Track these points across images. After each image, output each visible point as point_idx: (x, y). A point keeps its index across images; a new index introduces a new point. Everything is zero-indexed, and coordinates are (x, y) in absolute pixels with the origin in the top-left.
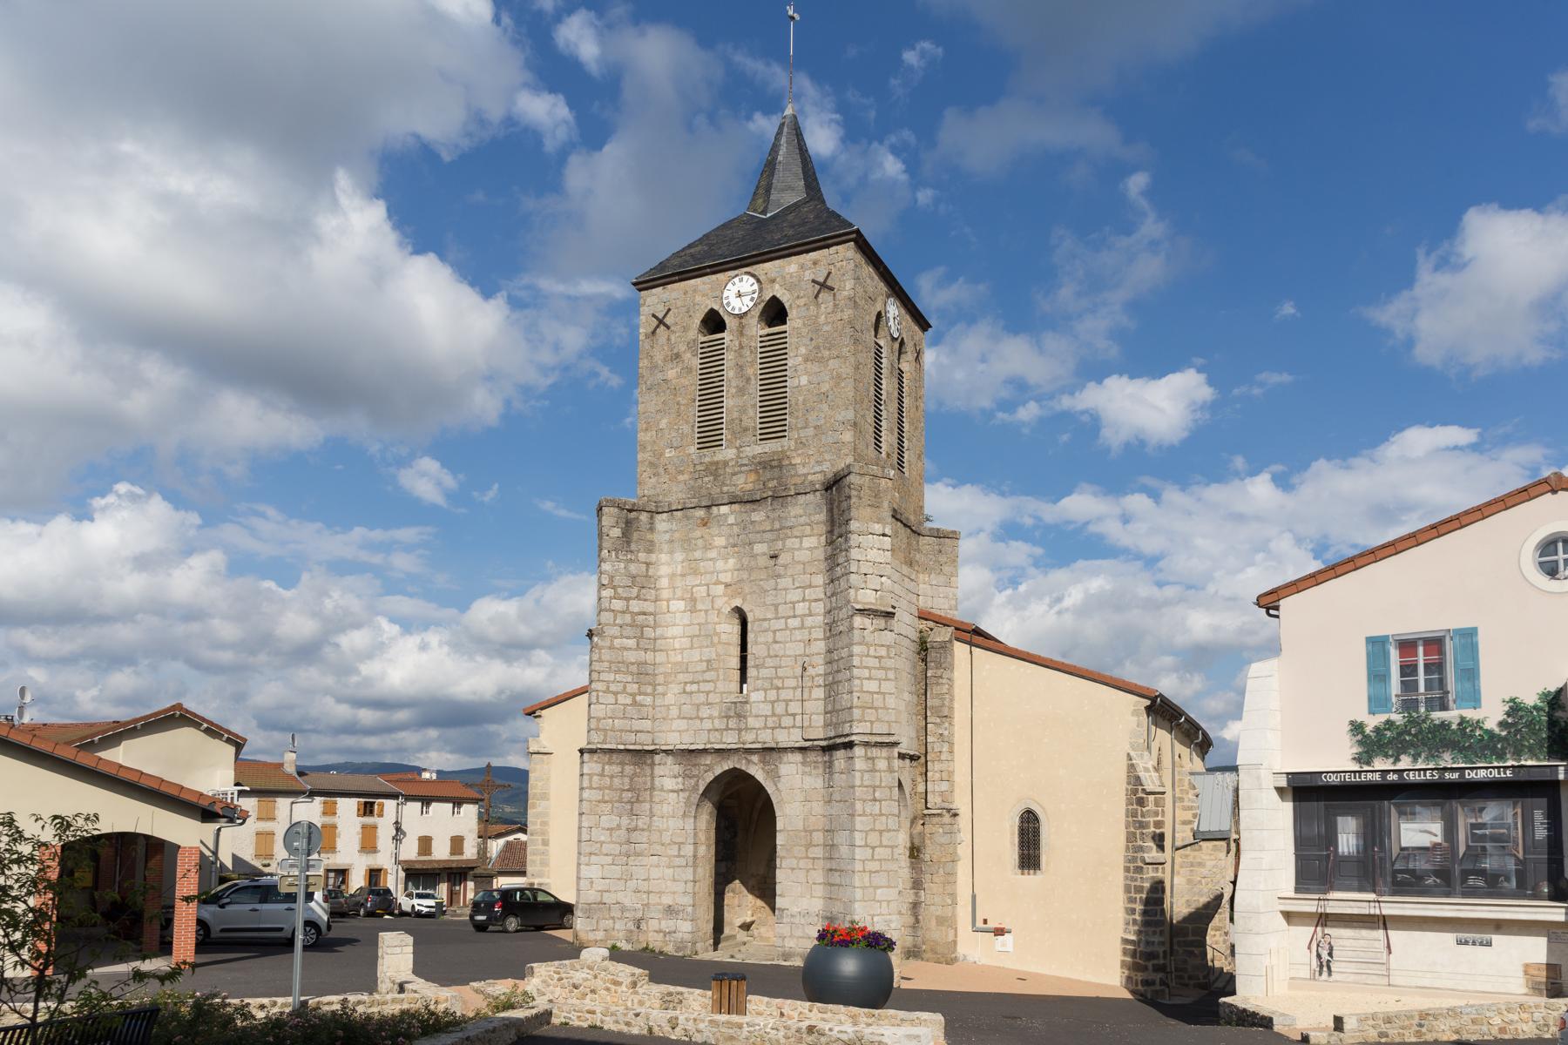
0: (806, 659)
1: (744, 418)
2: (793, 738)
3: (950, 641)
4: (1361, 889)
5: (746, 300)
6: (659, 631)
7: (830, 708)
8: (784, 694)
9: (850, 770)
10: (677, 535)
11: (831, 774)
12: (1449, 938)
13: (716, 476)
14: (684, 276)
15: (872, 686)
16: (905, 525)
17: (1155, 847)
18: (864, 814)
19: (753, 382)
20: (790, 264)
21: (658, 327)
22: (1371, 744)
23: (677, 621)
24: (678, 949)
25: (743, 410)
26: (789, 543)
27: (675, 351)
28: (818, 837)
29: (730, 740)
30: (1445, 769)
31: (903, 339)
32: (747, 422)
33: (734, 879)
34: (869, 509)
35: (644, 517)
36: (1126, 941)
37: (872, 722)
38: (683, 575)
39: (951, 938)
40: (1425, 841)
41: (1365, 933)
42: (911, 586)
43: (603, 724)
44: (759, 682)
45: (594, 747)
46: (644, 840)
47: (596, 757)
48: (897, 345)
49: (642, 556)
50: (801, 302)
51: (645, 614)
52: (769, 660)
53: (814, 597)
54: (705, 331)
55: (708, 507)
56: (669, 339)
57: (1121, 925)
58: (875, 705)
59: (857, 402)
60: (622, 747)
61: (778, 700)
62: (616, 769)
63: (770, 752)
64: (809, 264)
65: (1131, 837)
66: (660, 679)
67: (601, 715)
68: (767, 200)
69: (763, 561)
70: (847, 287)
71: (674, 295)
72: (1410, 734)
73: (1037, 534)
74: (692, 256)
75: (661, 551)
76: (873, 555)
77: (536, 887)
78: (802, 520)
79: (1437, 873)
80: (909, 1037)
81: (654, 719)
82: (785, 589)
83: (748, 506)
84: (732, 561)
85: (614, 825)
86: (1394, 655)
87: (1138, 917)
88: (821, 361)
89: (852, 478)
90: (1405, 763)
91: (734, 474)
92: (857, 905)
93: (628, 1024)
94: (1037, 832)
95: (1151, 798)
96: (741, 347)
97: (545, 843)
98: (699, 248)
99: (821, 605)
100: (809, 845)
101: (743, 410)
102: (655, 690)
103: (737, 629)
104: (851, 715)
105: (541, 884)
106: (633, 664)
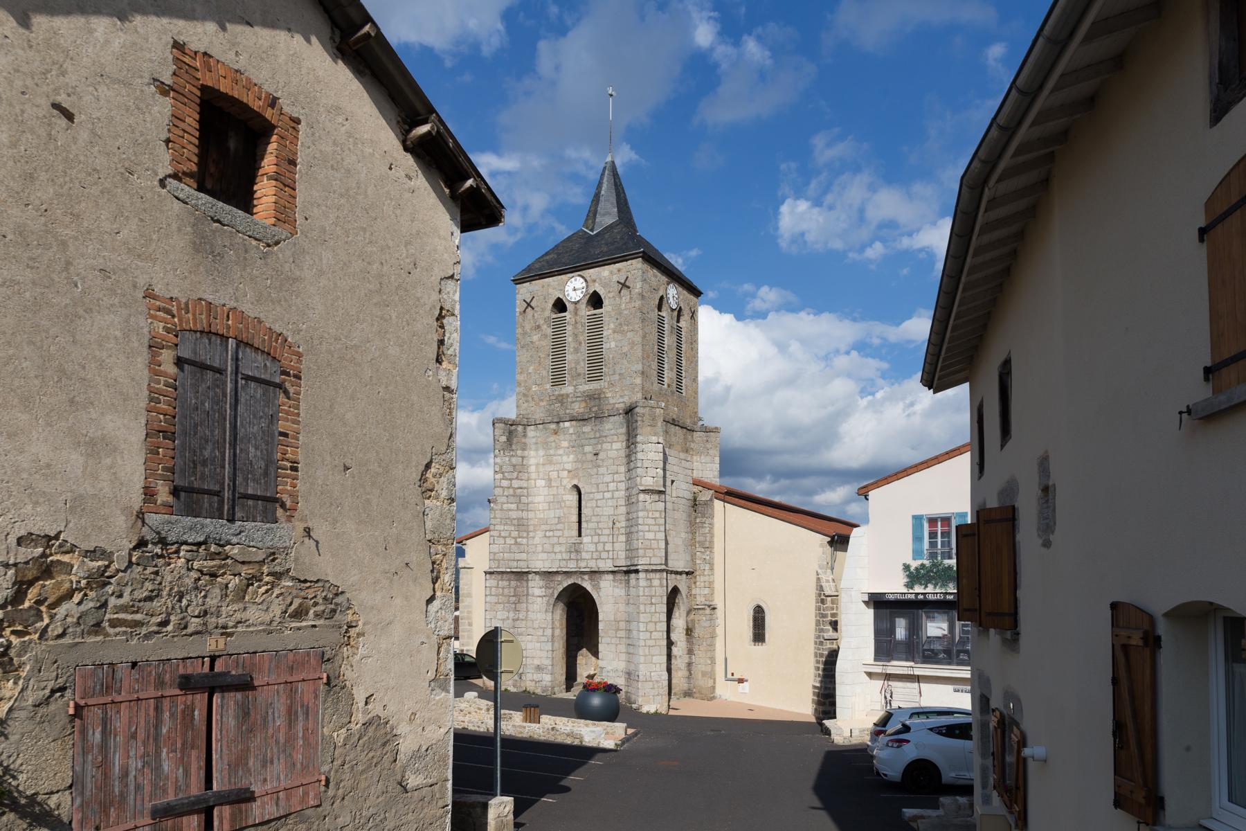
0: (615, 517)
1: (578, 367)
2: (607, 565)
3: (711, 500)
4: (907, 660)
5: (579, 292)
6: (530, 499)
7: (628, 547)
8: (603, 539)
9: (637, 586)
10: (539, 439)
11: (629, 587)
12: (950, 688)
13: (562, 403)
14: (542, 276)
15: (650, 536)
16: (682, 427)
17: (831, 629)
18: (645, 612)
19: (583, 344)
20: (604, 270)
21: (527, 308)
22: (914, 577)
23: (541, 493)
24: (543, 692)
25: (577, 363)
26: (605, 446)
27: (537, 324)
28: (622, 625)
29: (572, 566)
30: (946, 593)
31: (680, 308)
32: (580, 370)
33: (583, 648)
34: (649, 428)
35: (520, 428)
36: (815, 687)
37: (650, 558)
38: (543, 465)
39: (710, 683)
40: (939, 633)
41: (909, 685)
42: (688, 465)
43: (497, 556)
44: (588, 531)
45: (492, 570)
46: (524, 626)
47: (493, 576)
48: (676, 313)
49: (519, 453)
50: (611, 295)
51: (521, 488)
52: (593, 517)
53: (619, 480)
54: (556, 311)
55: (558, 423)
56: (533, 316)
57: (812, 677)
58: (653, 546)
59: (645, 357)
60: (509, 570)
61: (599, 542)
62: (506, 583)
63: (595, 574)
64: (616, 271)
65: (818, 624)
66: (531, 528)
67: (496, 551)
68: (594, 222)
69: (590, 457)
70: (637, 286)
71: (537, 288)
72: (933, 572)
73: (884, 352)
74: (547, 262)
75: (531, 449)
76: (652, 456)
77: (465, 652)
78: (612, 432)
79: (945, 651)
80: (591, 731)
81: (528, 553)
82: (603, 475)
83: (581, 423)
84: (572, 456)
85: (505, 617)
86: (926, 525)
87: (821, 672)
88: (622, 332)
89: (637, 410)
90: (930, 589)
91: (574, 402)
92: (641, 666)
93: (479, 727)
94: (763, 619)
95: (829, 599)
96: (576, 323)
97: (470, 624)
98: (551, 256)
99: (623, 484)
100: (618, 630)
101: (577, 363)
102: (528, 535)
103: (576, 497)
104: (638, 553)
105: (467, 650)
106: (514, 519)
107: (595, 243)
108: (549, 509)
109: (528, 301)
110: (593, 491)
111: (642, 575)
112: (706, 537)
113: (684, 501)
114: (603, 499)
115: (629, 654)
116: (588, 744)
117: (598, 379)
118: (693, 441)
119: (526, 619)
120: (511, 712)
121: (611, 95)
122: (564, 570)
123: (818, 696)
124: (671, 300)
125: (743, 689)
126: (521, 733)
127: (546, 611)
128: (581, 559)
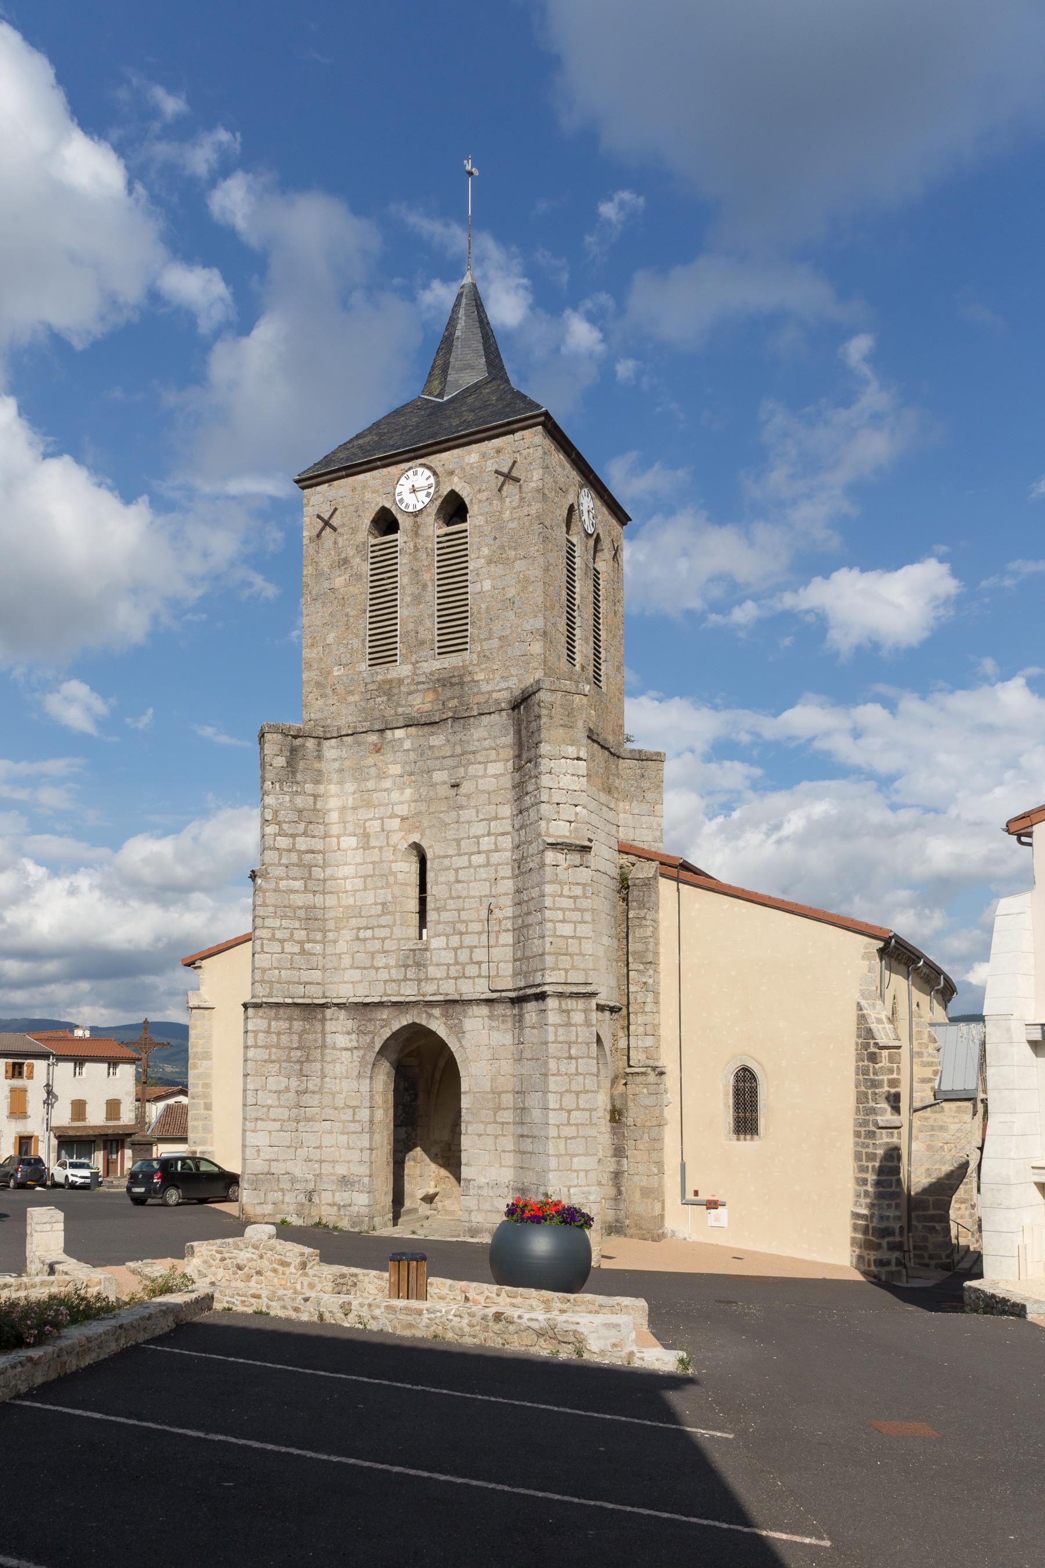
0: (492, 900)
1: (421, 629)
3: (655, 878)
5: (422, 495)
6: (329, 871)
7: (519, 954)
8: (468, 940)
9: (543, 1025)
10: (347, 763)
11: (521, 1028)
13: (389, 695)
15: (566, 930)
16: (603, 747)
17: (889, 1109)
18: (558, 1074)
19: (430, 588)
21: (323, 529)
23: (349, 860)
26: (472, 770)
27: (343, 556)
28: (508, 1100)
29: (408, 992)
31: (598, 535)
32: (424, 635)
33: (415, 1146)
34: (561, 730)
35: (311, 743)
36: (856, 1216)
37: (566, 971)
38: (353, 808)
45: (259, 1001)
46: (315, 1103)
47: (261, 1012)
49: (309, 787)
50: (483, 496)
51: (312, 852)
52: (451, 902)
54: (376, 532)
55: (382, 731)
56: (335, 543)
57: (851, 1197)
60: (289, 1001)
61: (461, 947)
62: (284, 1025)
64: (492, 453)
65: (861, 1098)
66: (331, 924)
67: (266, 964)
68: (444, 382)
69: (444, 791)
70: (534, 478)
71: (341, 492)
73: (755, 753)
74: (360, 447)
75: (330, 781)
77: (198, 1155)
78: (487, 743)
80: (607, 1326)
81: (324, 969)
82: (469, 822)
83: (426, 729)
84: (408, 792)
85: (282, 1087)
87: (870, 1188)
88: (506, 562)
89: (542, 695)
91: (410, 693)
92: (551, 1175)
93: (296, 1310)
94: (754, 1092)
95: (885, 1053)
96: (416, 549)
97: (208, 1107)
100: (498, 1108)
101: (419, 621)
103: (415, 867)
104: (543, 962)
105: (203, 1153)
106: (300, 908)
107: (448, 413)
108: (365, 889)
109: (326, 516)
110: (450, 853)
111: (551, 1003)
112: (647, 943)
113: (605, 880)
114: (470, 866)
115: (524, 1153)
116: (596, 1359)
117: (460, 648)
118: (618, 776)
119: (320, 1091)
120: (354, 1270)
121: (471, 174)
122: (394, 999)
123: (866, 1230)
124: (585, 517)
125: (717, 1220)
126: (410, 1326)
127: (359, 1076)
128: (427, 979)
